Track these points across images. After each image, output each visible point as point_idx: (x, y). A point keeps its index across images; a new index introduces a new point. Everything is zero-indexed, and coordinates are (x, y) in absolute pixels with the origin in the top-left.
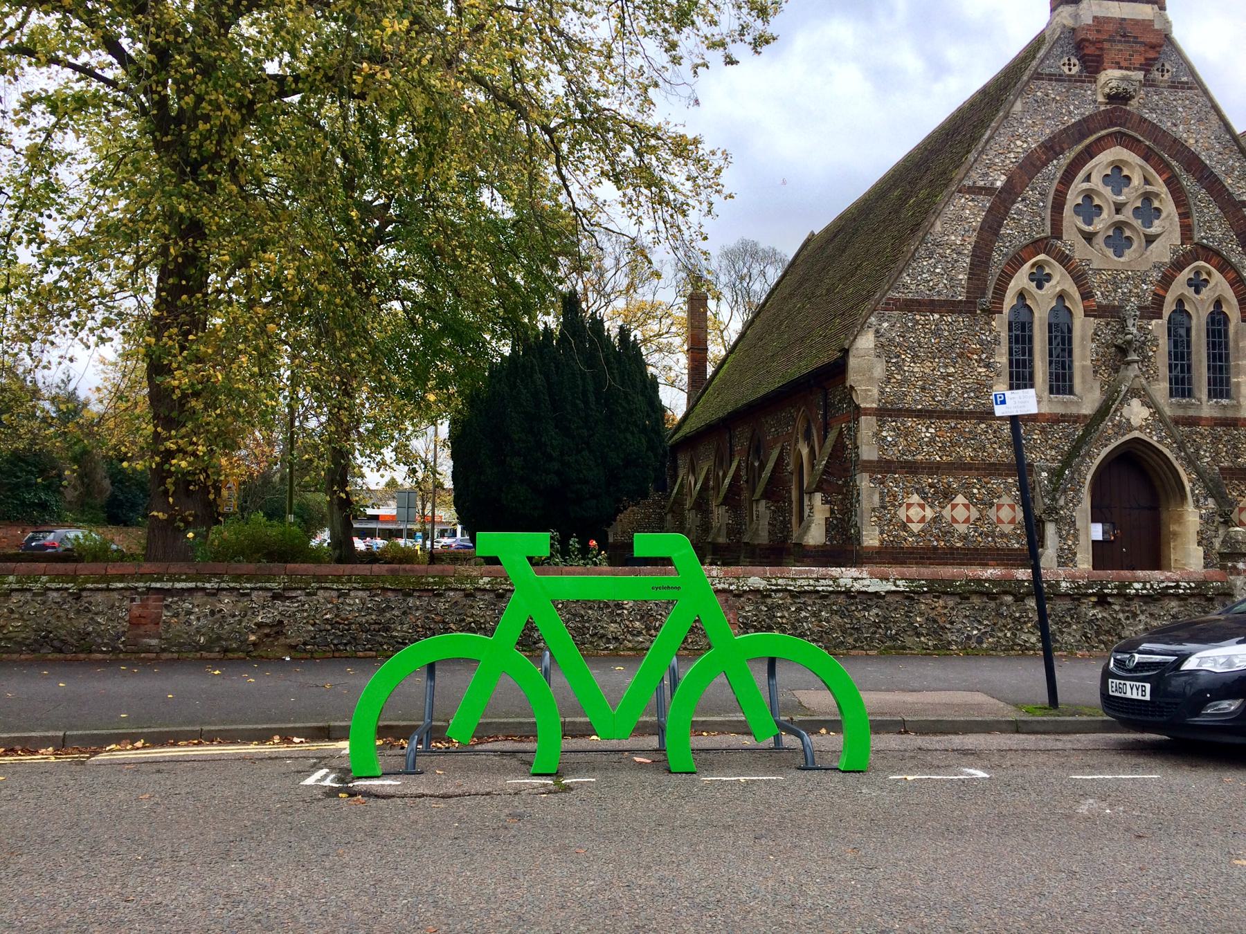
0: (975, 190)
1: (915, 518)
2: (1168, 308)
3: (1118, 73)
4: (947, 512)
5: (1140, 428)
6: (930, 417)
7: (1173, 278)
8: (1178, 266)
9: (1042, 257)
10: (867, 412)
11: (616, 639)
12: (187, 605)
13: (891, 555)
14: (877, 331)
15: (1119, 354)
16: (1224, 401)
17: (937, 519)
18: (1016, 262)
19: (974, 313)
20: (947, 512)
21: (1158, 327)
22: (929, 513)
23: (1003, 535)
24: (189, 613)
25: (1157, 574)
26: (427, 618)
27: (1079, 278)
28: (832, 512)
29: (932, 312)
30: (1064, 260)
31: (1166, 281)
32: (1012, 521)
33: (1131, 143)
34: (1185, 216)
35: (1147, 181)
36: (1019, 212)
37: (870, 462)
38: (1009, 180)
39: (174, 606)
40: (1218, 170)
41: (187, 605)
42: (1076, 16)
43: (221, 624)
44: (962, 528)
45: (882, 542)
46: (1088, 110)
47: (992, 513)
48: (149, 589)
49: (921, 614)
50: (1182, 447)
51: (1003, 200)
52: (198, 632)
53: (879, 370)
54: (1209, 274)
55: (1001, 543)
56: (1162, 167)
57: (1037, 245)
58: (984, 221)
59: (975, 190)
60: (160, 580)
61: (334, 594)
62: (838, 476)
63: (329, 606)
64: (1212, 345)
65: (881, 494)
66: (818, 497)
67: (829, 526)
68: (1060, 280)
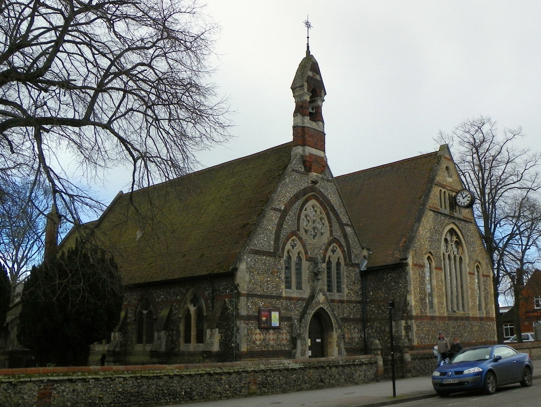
0: (275, 209)
1: (258, 339)
2: (327, 259)
3: (315, 174)
4: (267, 337)
5: (322, 304)
6: (262, 298)
7: (328, 249)
8: (329, 244)
9: (294, 237)
10: (243, 295)
11: (220, 393)
12: (63, 388)
13: (252, 354)
14: (247, 262)
15: (315, 275)
16: (340, 294)
17: (264, 340)
18: (288, 239)
19: (275, 257)
20: (267, 337)
21: (324, 265)
22: (262, 337)
23: (284, 345)
24: (63, 391)
25: (322, 359)
26: (156, 388)
27: (304, 246)
28: (221, 336)
29: (263, 255)
30: (300, 239)
31: (326, 250)
32: (286, 339)
33: (317, 199)
34: (331, 227)
35: (321, 214)
36: (288, 220)
37: (244, 316)
38: (285, 208)
39: (58, 388)
40: (339, 212)
41: (63, 388)
42: (304, 151)
43: (77, 396)
44: (272, 343)
45: (247, 349)
46: (306, 185)
47: (280, 336)
48: (49, 380)
49: (306, 375)
50: (332, 311)
51: (284, 214)
52: (67, 400)
53: (247, 278)
54: (336, 248)
55: (283, 348)
56: (325, 208)
57: (294, 233)
58: (278, 222)
59: (275, 209)
60: (52, 376)
61: (122, 379)
62: (227, 322)
63: (120, 385)
64: (297, 269)
65: (248, 329)
66: (217, 330)
67: (221, 343)
68: (299, 247)
